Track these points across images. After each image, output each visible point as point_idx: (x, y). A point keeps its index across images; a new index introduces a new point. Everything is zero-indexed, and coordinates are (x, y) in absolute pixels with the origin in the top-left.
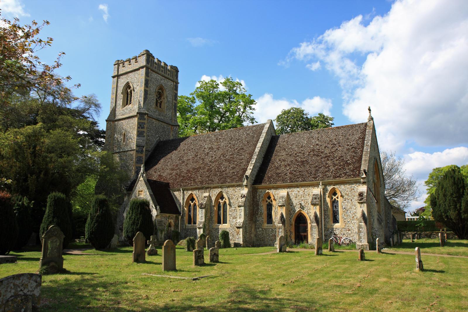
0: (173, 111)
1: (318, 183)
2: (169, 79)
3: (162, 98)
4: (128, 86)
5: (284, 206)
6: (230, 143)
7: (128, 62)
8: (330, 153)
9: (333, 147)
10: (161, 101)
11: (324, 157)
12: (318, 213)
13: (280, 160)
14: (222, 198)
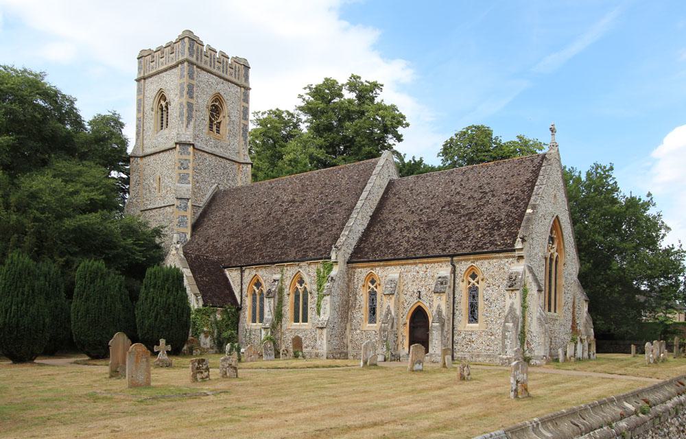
0: (242, 139)
3: (221, 116)
4: (162, 96)
9: (481, 198)
10: (218, 121)
11: (464, 216)
12: (443, 308)
13: (395, 220)
14: (301, 282)
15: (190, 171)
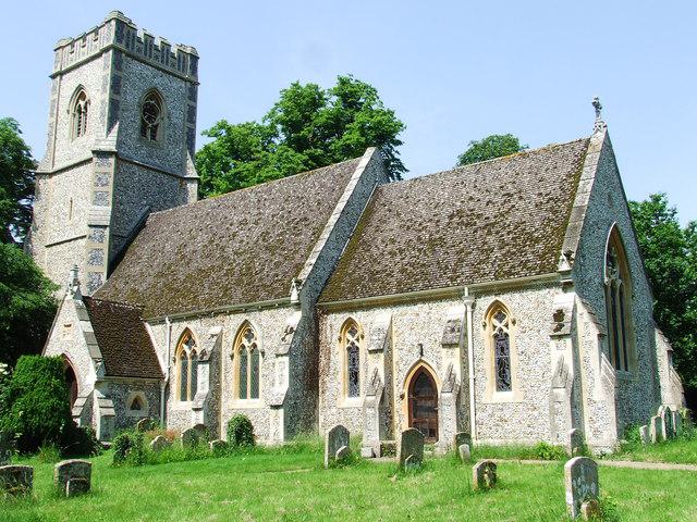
1: (459, 291)
2: (175, 75)
4: (80, 93)
5: (381, 351)
6: (283, 209)
7: (81, 41)
8: (495, 217)
15: (110, 189)
